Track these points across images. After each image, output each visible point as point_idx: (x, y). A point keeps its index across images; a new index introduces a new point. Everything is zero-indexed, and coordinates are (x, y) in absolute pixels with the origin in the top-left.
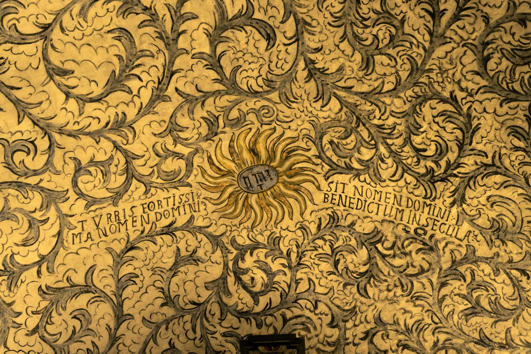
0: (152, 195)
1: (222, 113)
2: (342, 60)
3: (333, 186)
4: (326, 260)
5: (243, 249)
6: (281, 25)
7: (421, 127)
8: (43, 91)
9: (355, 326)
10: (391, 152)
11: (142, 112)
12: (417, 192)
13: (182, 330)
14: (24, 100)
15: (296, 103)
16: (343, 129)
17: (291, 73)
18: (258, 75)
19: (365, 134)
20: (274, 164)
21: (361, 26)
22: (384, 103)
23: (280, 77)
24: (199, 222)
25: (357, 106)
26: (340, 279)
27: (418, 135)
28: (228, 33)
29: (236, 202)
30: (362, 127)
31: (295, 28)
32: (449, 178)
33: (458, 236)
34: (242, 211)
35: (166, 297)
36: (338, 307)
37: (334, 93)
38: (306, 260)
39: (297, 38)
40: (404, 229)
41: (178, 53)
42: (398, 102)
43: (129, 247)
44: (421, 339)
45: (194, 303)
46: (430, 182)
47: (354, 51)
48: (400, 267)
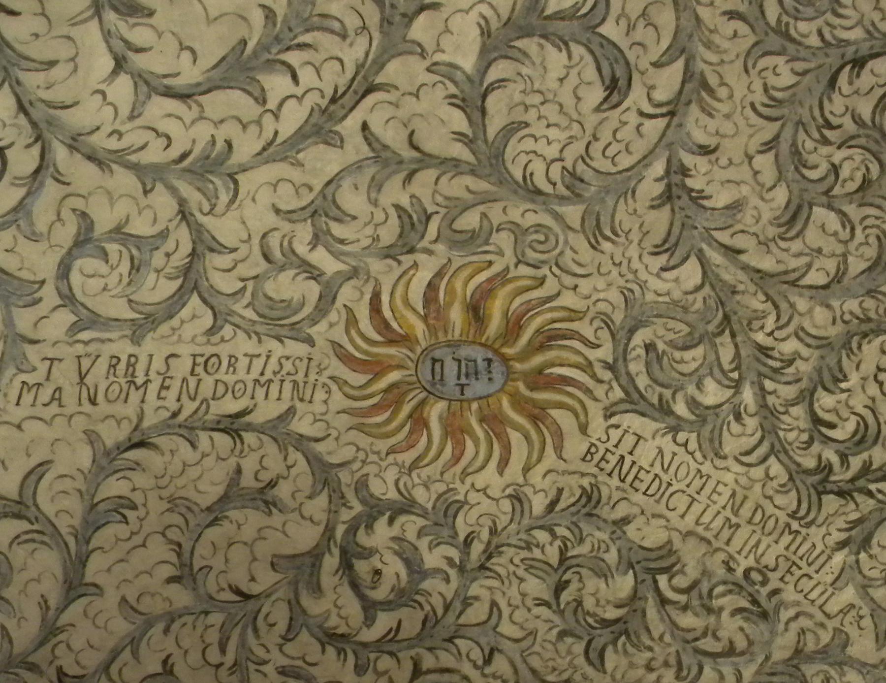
0: (223, 340)
1: (443, 211)
2: (745, 190)
3: (615, 434)
4: (541, 574)
5: (377, 505)
6: (652, 70)
7: (845, 378)
8: (69, 38)
10: (764, 406)
11: (269, 153)
12: (779, 500)
14: (17, 46)
15: (613, 242)
16: (686, 329)
17: (629, 178)
18: (557, 156)
19: (727, 354)
20: (508, 351)
21: (816, 136)
22: (792, 306)
23: (602, 177)
24: (303, 426)
25: (734, 292)
26: (556, 619)
27: (832, 392)
28: (530, 45)
29: (398, 404)
30: (726, 337)
31: (677, 87)
32: (855, 494)
33: (825, 608)
34: (402, 426)
35: (182, 565)
36: (533, 671)
37: (701, 250)
38: (499, 564)
39: (672, 111)
40: (726, 563)
41: (402, 47)
42: (821, 315)
43: (135, 440)
45: (238, 592)
46: (815, 489)
47: (779, 180)
48: (689, 631)
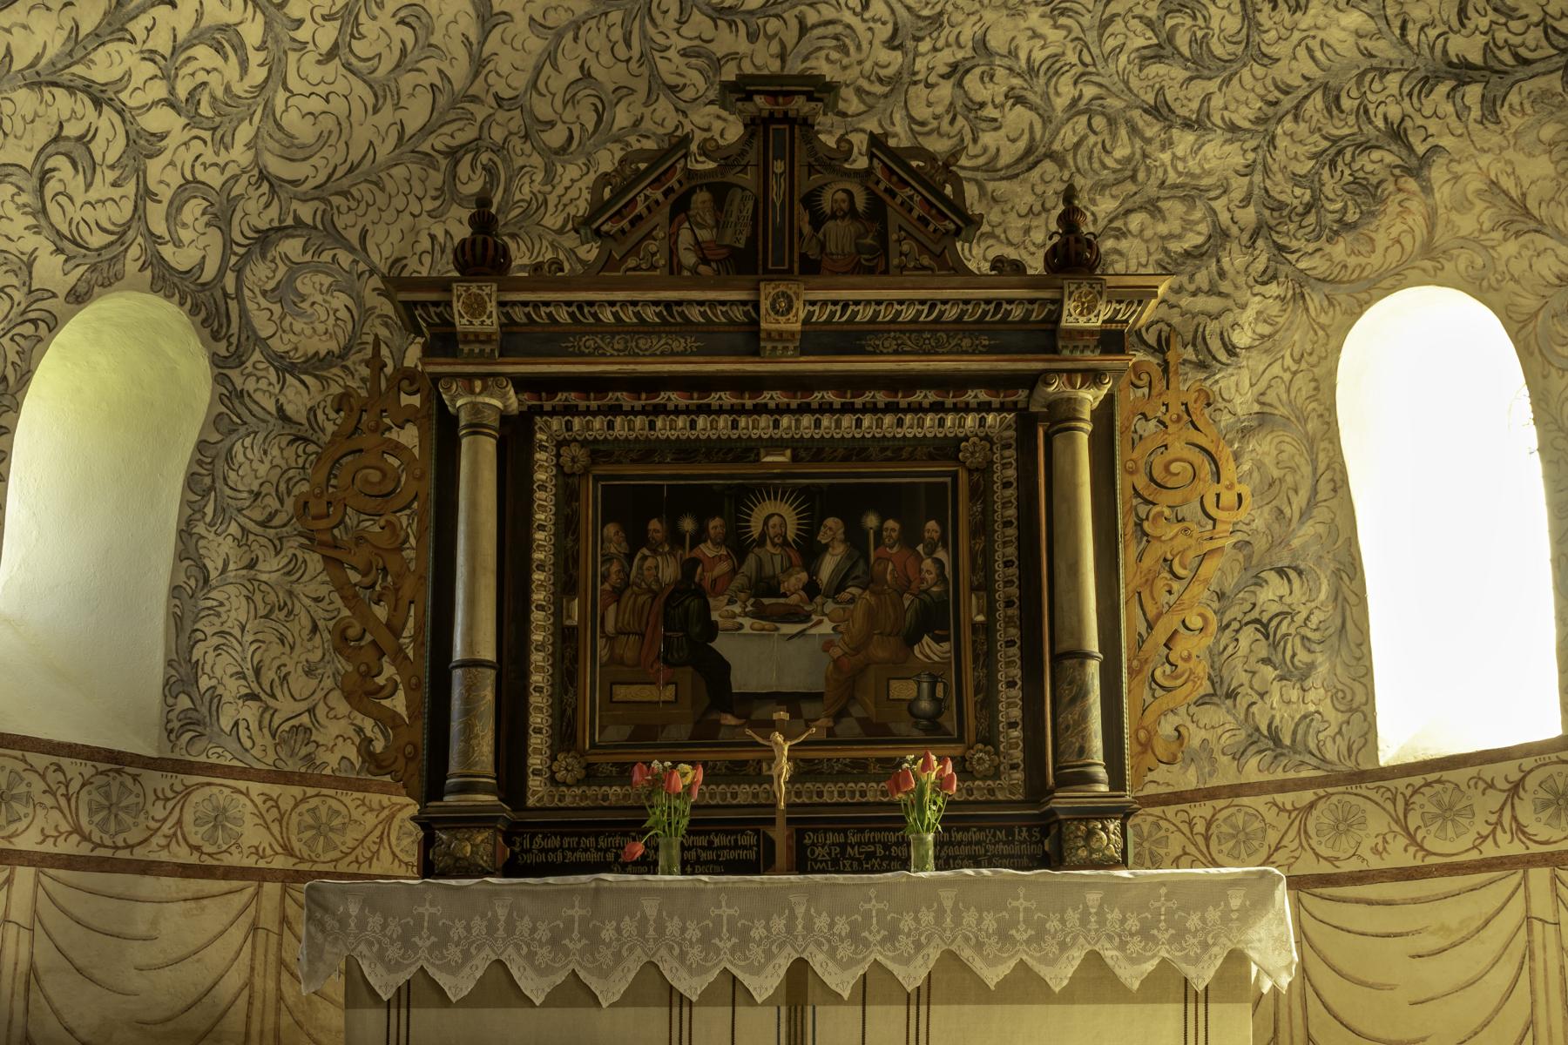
9: (935, 49)
13: (605, 40)
44: (1051, 91)
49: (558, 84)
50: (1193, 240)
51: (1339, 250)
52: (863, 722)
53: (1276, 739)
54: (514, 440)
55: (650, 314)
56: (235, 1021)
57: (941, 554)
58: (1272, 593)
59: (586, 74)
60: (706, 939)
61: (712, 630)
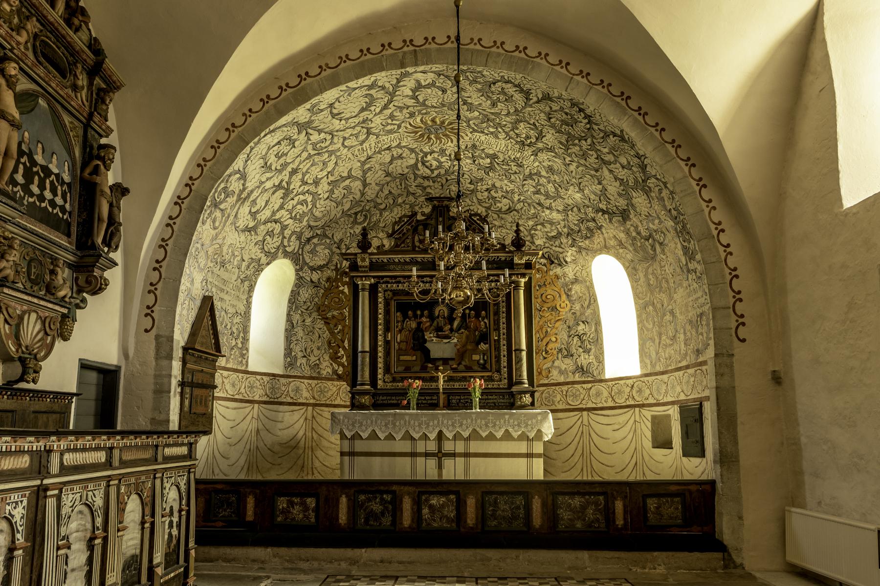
24: (404, 144)
49: (383, 195)
50: (553, 234)
51: (587, 242)
52: (465, 366)
53: (582, 368)
54: (373, 290)
55: (408, 260)
56: (302, 443)
57: (486, 320)
58: (581, 328)
59: (390, 192)
60: (419, 425)
61: (425, 341)
